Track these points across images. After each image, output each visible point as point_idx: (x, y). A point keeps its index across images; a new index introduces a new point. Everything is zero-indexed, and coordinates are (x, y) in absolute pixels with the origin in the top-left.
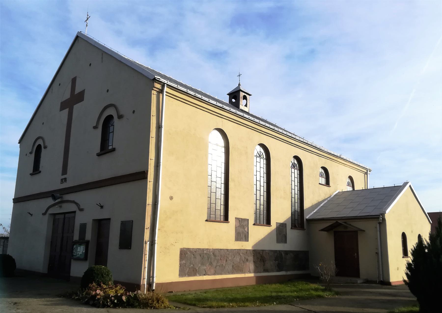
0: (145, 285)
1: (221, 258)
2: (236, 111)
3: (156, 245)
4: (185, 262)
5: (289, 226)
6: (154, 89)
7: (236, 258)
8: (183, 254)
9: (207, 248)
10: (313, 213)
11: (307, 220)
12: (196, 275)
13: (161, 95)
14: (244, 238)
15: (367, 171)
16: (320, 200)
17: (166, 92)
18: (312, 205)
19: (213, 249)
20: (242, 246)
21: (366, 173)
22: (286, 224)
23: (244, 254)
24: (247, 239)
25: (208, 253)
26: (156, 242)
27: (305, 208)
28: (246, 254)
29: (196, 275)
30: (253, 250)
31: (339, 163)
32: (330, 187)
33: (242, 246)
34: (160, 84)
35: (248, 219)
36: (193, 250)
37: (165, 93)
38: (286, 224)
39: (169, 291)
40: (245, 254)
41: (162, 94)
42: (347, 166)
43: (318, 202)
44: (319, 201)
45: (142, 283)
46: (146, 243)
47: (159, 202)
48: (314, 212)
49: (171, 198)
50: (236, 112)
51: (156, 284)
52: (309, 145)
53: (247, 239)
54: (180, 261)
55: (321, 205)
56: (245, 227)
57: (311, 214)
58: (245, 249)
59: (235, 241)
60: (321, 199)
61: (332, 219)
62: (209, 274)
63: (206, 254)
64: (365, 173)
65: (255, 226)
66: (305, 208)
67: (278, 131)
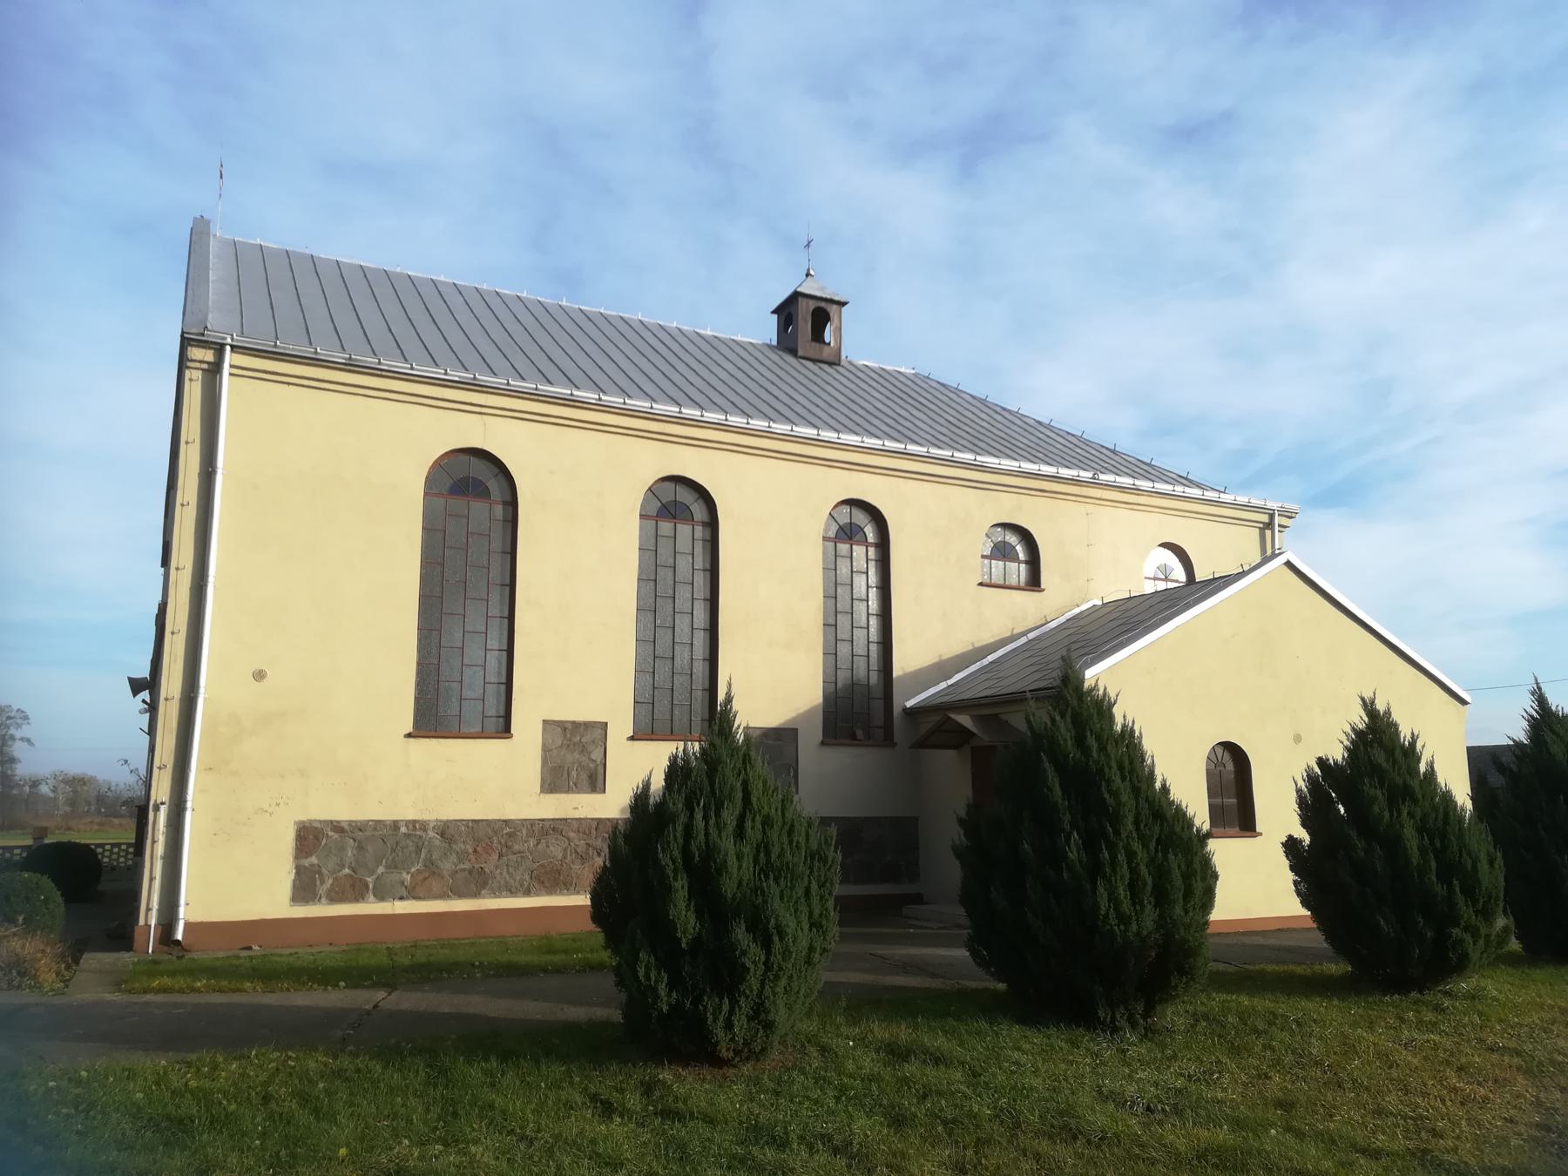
0: (150, 926)
1: (479, 849)
2: (570, 392)
3: (188, 815)
4: (319, 859)
5: (810, 738)
6: (189, 364)
7: (548, 846)
8: (311, 837)
9: (411, 817)
10: (943, 685)
11: (907, 711)
12: (363, 899)
13: (1268, 533)
14: (585, 783)
15: (1272, 516)
16: (987, 638)
17: (1279, 526)
18: (936, 660)
19: (441, 821)
20: (575, 808)
21: (1269, 525)
22: (797, 729)
23: (584, 833)
24: (595, 781)
25: (415, 835)
26: (189, 805)
27: (895, 674)
28: (594, 832)
29: (363, 899)
30: (625, 819)
31: (1073, 498)
32: (1043, 590)
33: (575, 808)
34: (210, 348)
35: (606, 724)
36: (350, 825)
37: (1277, 528)
38: (797, 729)
39: (245, 946)
40: (587, 832)
41: (1270, 531)
42: (1149, 509)
43: (971, 648)
44: (977, 645)
45: (142, 922)
46: (157, 808)
47: (202, 690)
48: (950, 682)
49: (259, 675)
50: (536, 389)
51: (187, 925)
52: (279, 357)
53: (595, 781)
54: (297, 857)
55: (991, 658)
56: (591, 748)
57: (932, 691)
58: (589, 817)
59: (542, 792)
60: (992, 636)
61: (982, 705)
62: (421, 895)
63: (408, 836)
64: (1261, 525)
65: (636, 743)
66: (901, 673)
67: (1174, 493)
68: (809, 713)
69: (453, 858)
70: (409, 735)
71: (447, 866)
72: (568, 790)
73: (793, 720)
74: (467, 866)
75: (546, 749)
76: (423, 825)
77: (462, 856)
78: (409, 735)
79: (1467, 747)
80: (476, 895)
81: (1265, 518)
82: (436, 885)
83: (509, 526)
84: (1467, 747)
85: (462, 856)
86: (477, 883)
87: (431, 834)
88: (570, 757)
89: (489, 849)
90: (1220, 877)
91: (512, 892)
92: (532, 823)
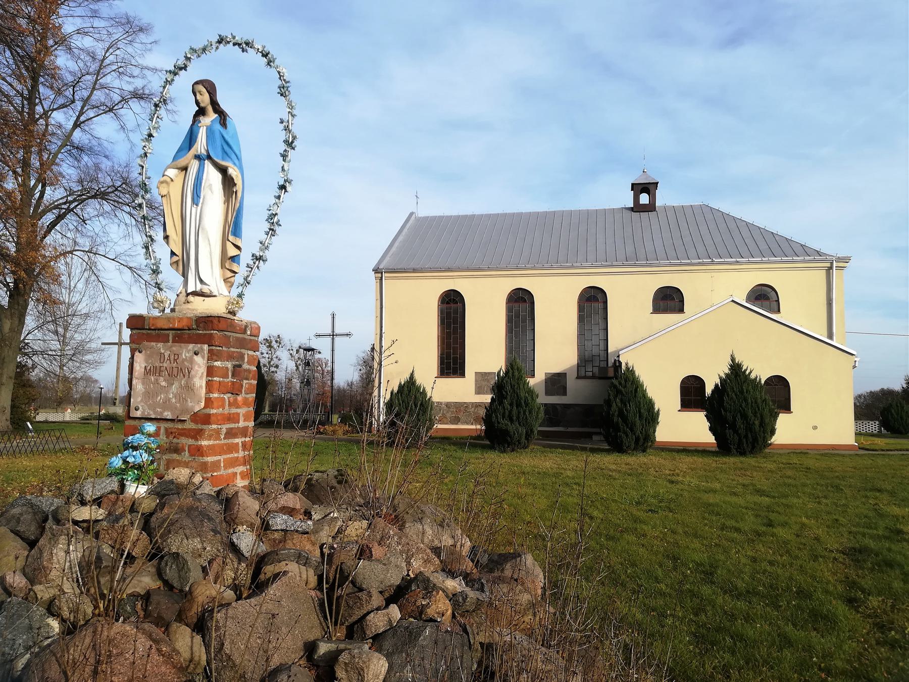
15: (832, 263)
49: (815, 428)
68: (571, 368)
69: (450, 413)
70: (679, 411)
71: (448, 415)
72: (484, 394)
73: (565, 370)
74: (454, 415)
75: (476, 381)
76: (441, 403)
77: (452, 412)
78: (679, 411)
79: (681, 310)
80: (457, 424)
81: (828, 265)
82: (445, 420)
83: (606, 331)
84: (681, 310)
85: (452, 412)
86: (456, 420)
87: (443, 406)
88: (484, 383)
89: (460, 411)
90: (661, 419)
91: (467, 424)
92: (473, 403)
